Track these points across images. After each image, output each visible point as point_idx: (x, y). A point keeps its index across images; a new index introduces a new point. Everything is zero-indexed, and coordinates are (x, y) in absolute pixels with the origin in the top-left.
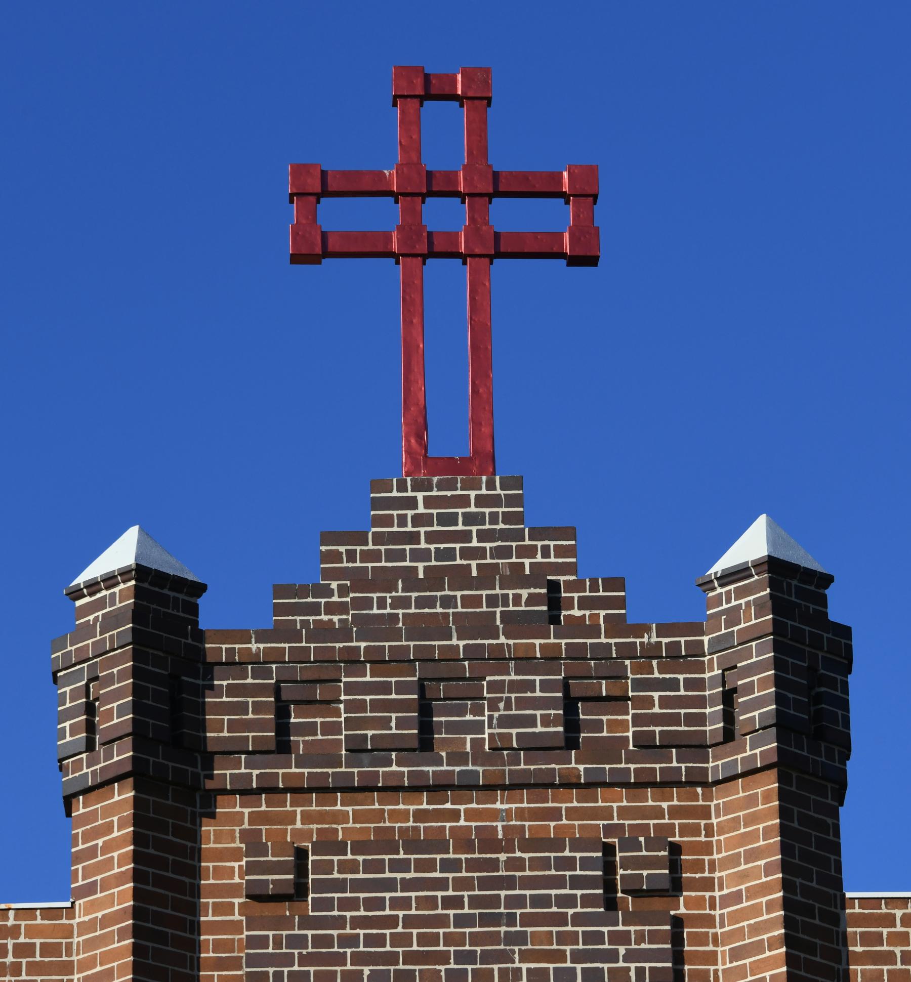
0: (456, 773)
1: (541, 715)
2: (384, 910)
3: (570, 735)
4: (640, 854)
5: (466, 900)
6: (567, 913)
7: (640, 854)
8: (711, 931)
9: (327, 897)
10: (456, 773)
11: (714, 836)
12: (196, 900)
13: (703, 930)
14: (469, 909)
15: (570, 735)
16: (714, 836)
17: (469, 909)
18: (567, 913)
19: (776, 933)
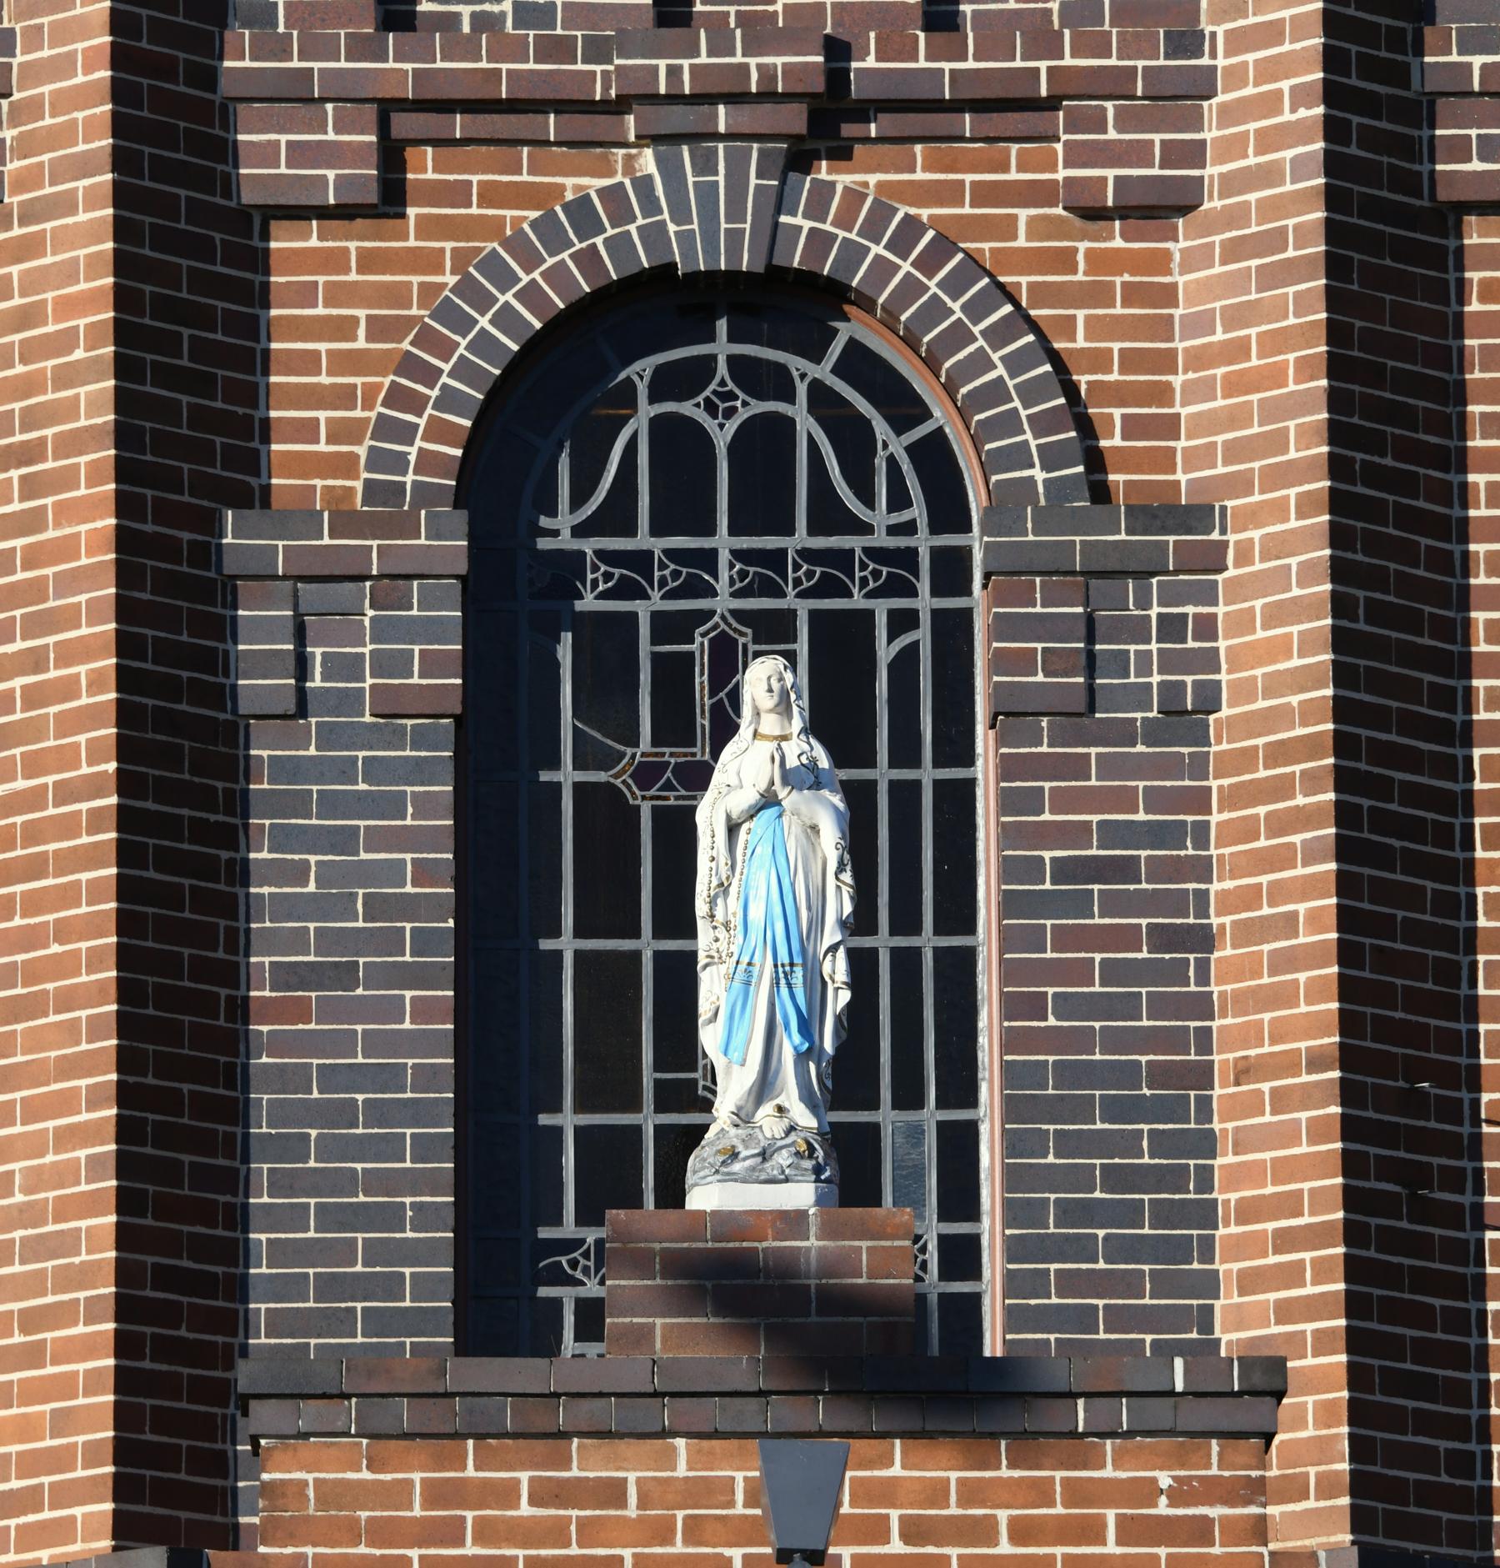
0: (1164, 378)
1: (1115, 307)
2: (363, 1030)
3: (934, 8)
4: (1437, 886)
5: (1080, 257)
6: (878, 59)
7: (1437, 886)
8: (220, 167)
9: (161, 252)
10: (1164, 378)
11: (1179, 439)
12: (240, 959)
13: (330, 244)
14: (416, 239)
15: (934, 8)
16: (1179, 439)
17: (416, 239)
18: (878, 59)
19: (99, 524)
